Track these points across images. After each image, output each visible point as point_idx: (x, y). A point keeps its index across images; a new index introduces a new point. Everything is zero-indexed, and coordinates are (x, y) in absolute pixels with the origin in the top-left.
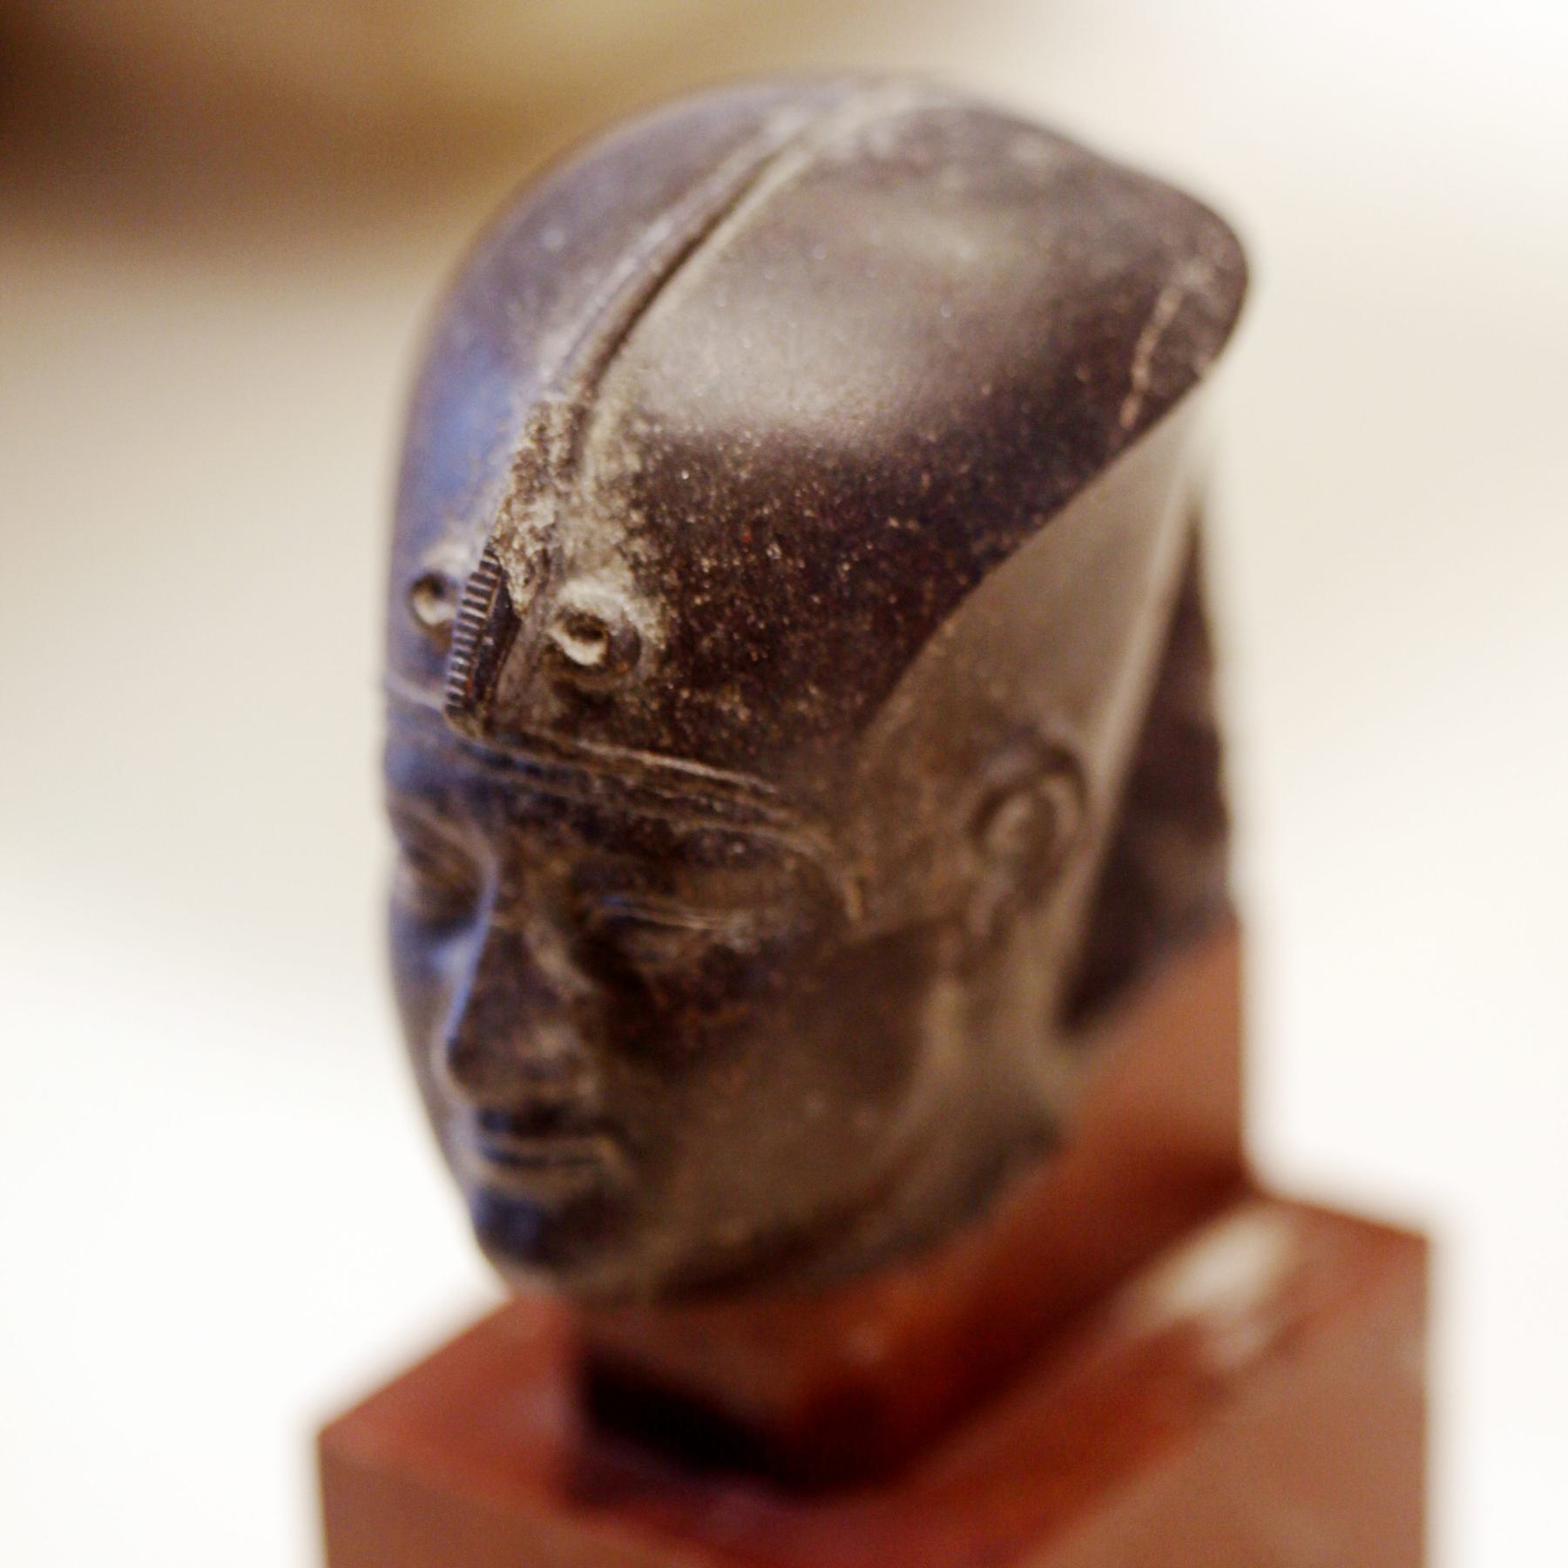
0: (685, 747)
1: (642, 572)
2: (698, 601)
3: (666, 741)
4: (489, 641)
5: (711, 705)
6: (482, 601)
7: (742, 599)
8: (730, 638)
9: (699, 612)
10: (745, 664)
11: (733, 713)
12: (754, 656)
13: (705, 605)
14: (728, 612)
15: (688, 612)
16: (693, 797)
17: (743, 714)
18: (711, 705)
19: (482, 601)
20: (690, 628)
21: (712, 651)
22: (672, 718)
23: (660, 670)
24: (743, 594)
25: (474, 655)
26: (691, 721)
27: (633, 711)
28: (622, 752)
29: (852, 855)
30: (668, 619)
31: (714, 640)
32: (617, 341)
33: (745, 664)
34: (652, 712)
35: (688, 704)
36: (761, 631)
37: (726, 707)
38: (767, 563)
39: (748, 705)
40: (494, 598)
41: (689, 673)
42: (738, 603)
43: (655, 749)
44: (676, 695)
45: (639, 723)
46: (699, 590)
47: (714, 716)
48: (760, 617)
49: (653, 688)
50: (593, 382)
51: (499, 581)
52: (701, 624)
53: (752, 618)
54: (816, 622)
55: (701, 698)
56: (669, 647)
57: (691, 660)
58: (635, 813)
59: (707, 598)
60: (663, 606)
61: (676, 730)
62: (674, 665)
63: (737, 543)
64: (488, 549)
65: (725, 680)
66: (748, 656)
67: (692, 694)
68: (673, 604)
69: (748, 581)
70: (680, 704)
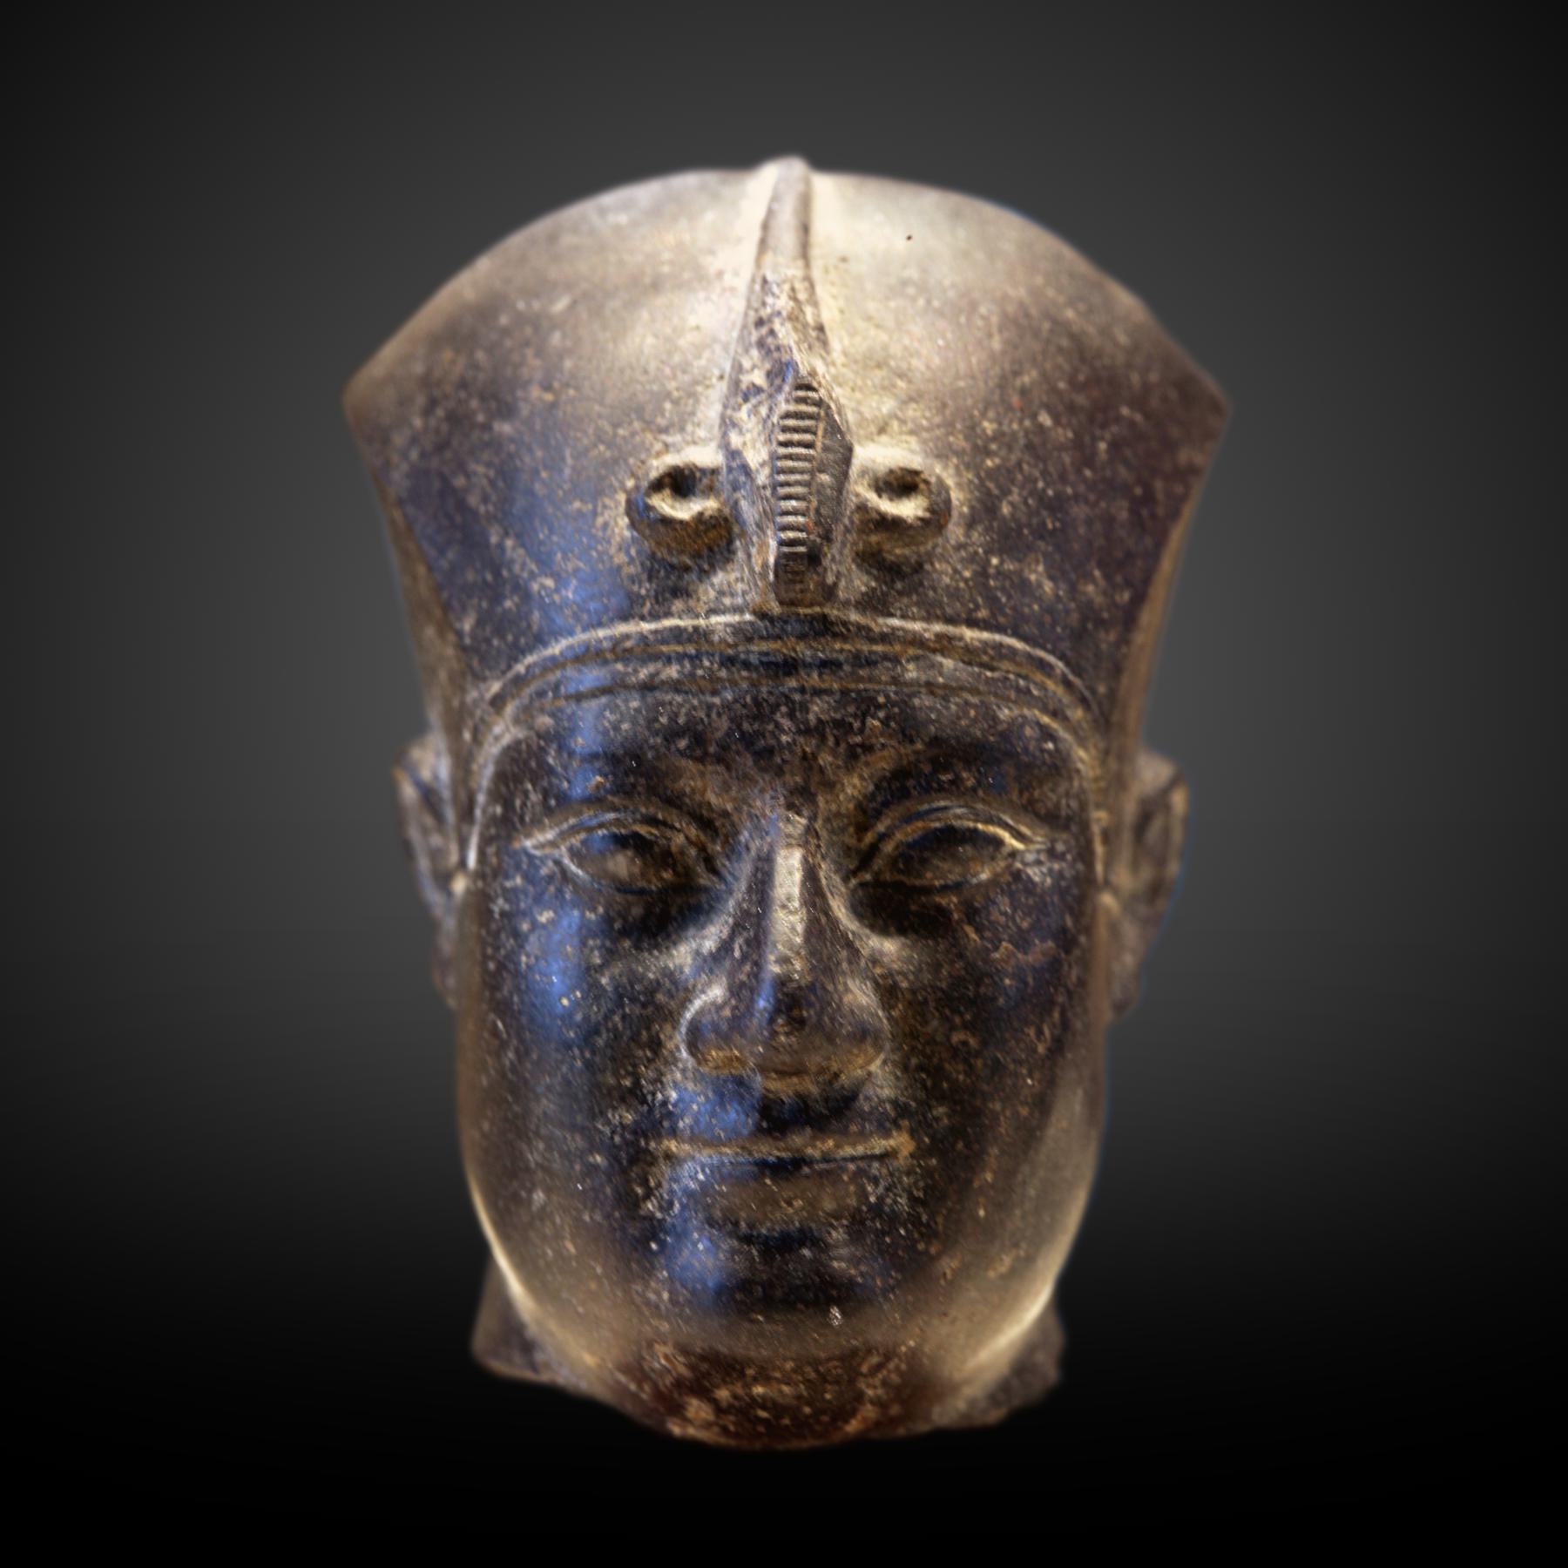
0: (1002, 620)
1: (925, 435)
2: (989, 463)
3: (983, 613)
4: (825, 478)
5: (1019, 573)
6: (808, 437)
8: (1026, 503)
9: (991, 474)
10: (1041, 532)
11: (1040, 585)
12: (1050, 526)
13: (998, 468)
14: (1019, 477)
15: (983, 474)
16: (645, 1091)
17: (1048, 586)
18: (1019, 573)
19: (808, 437)
20: (989, 490)
21: (1013, 515)
22: (986, 586)
23: (967, 535)
25: (810, 493)
26: (1003, 589)
27: (947, 580)
28: (938, 627)
30: (965, 480)
31: (1012, 504)
32: (805, 229)
33: (1041, 532)
34: (966, 581)
35: (999, 573)
36: (1050, 498)
37: (1033, 577)
38: (1041, 427)
39: (1051, 578)
40: (820, 433)
41: (995, 536)
42: (1025, 467)
43: (972, 623)
45: (954, 594)
46: (989, 453)
47: (1024, 586)
48: (1047, 484)
49: (963, 553)
50: (807, 265)
52: (999, 486)
53: (1041, 485)
55: (1010, 566)
56: (972, 508)
57: (995, 524)
58: (824, 834)
59: (997, 461)
60: (957, 468)
61: (992, 601)
62: (980, 528)
64: (698, 474)
65: (1030, 548)
66: (1044, 524)
67: (1002, 562)
68: (968, 467)
70: (992, 571)
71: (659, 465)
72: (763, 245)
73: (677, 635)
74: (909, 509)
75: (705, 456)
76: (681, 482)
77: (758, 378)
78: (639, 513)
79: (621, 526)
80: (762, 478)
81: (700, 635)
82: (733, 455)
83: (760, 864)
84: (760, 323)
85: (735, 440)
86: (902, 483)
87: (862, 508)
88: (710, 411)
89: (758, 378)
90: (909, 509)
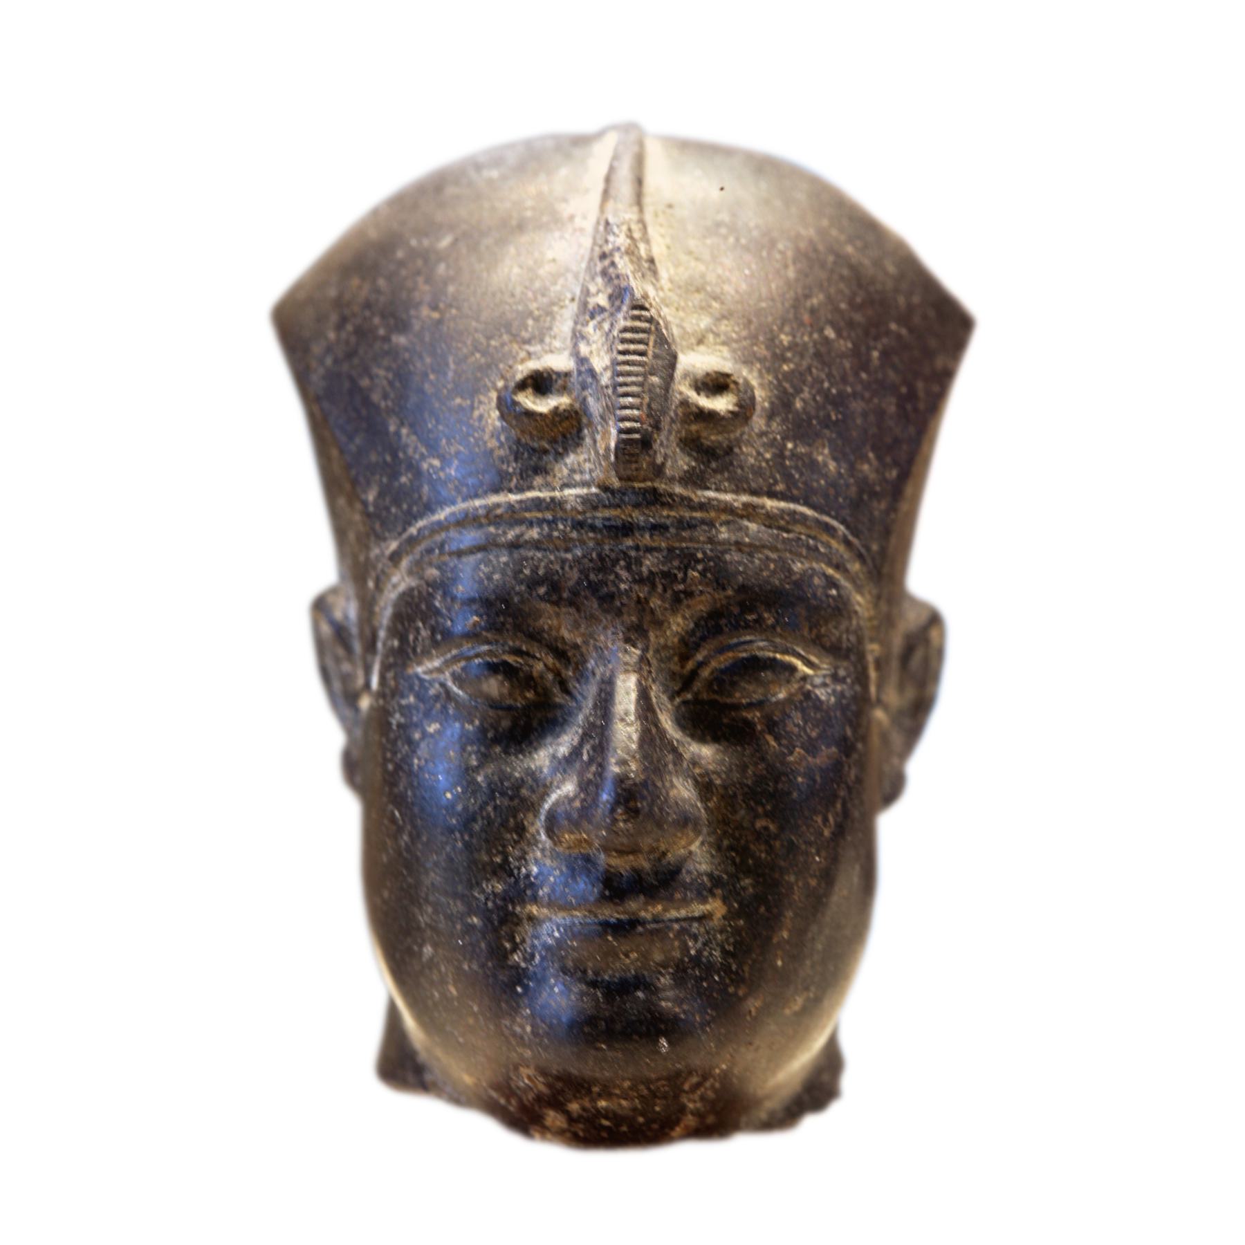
0: (795, 492)
1: (734, 345)
2: (785, 368)
3: (780, 487)
4: (655, 379)
5: (809, 455)
6: (641, 347)
7: (817, 368)
8: (814, 399)
11: (826, 465)
12: (834, 418)
13: (792, 371)
14: (809, 379)
15: (780, 376)
16: (512, 867)
17: (832, 466)
18: (809, 455)
19: (641, 347)
20: (785, 389)
21: (804, 409)
22: (783, 465)
23: (768, 425)
24: (815, 363)
25: (643, 392)
26: (797, 468)
27: (752, 460)
28: (745, 498)
29: (747, 841)
31: (803, 400)
32: (639, 182)
33: (826, 423)
34: (767, 461)
35: (794, 455)
36: (833, 396)
37: (820, 458)
39: (835, 459)
40: (651, 344)
41: (790, 426)
42: (814, 371)
43: (772, 495)
44: (785, 446)
45: (758, 472)
46: (785, 360)
47: (813, 465)
48: (832, 385)
51: (653, 328)
53: (826, 385)
54: (867, 395)
55: (802, 449)
56: (772, 403)
57: (790, 416)
58: (654, 662)
59: (792, 366)
60: (760, 371)
61: (788, 477)
62: (778, 419)
63: (801, 324)
65: (818, 435)
66: (829, 416)
67: (795, 446)
68: (768, 371)
69: (817, 355)
70: (787, 453)
71: (523, 369)
72: (606, 194)
73: (538, 504)
74: (722, 404)
75: (560, 362)
76: (541, 383)
77: (602, 300)
78: (507, 408)
79: (493, 417)
80: (605, 379)
81: (556, 504)
82: (582, 361)
83: (603, 686)
84: (603, 256)
85: (584, 349)
86: (716, 384)
87: (685, 403)
88: (564, 326)
89: (602, 300)
90: (722, 404)
